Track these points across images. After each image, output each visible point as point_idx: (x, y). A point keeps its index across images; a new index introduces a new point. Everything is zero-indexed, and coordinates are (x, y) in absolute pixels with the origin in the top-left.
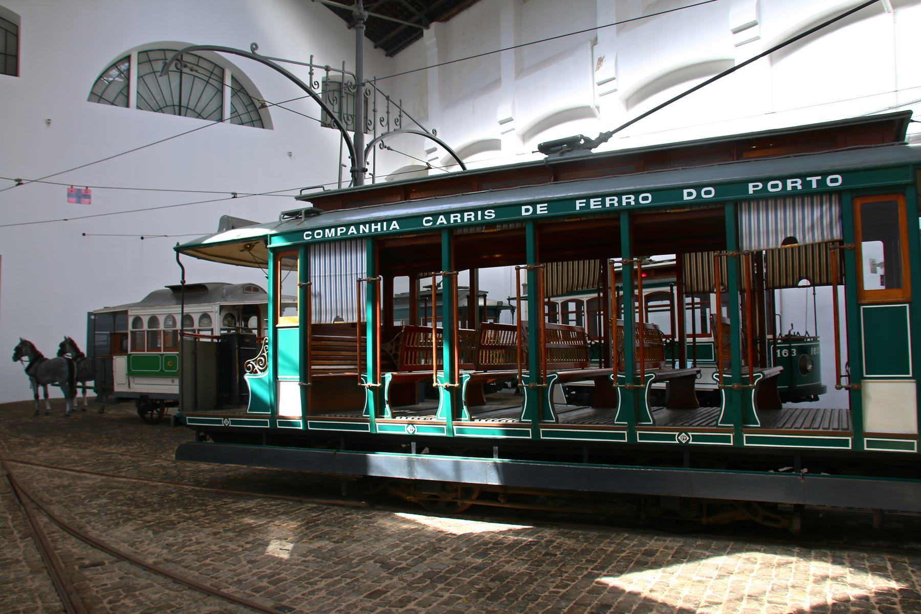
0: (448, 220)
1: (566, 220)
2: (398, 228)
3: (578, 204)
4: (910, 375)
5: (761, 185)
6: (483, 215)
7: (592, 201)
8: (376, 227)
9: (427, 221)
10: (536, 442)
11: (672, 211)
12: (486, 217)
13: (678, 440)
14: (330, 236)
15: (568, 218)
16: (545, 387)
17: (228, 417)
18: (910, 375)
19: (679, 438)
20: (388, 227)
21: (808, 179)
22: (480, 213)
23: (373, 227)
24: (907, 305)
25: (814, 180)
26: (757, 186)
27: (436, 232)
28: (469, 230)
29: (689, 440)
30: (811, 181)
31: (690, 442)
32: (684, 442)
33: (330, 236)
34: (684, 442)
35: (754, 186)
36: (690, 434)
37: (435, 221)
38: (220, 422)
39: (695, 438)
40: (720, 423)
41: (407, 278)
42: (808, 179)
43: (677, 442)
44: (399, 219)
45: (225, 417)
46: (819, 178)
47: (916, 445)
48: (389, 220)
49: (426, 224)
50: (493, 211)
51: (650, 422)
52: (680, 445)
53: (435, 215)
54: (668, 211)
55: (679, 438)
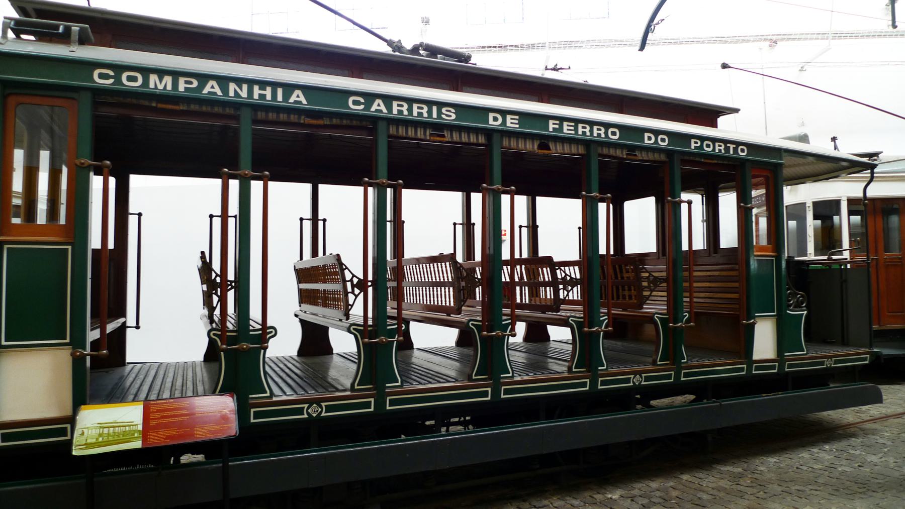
0: (389, 108)
1: (703, 160)
2: (305, 102)
3: (552, 125)
4: (68, 341)
5: (195, 84)
6: (439, 113)
7: (565, 124)
8: (262, 92)
9: (356, 103)
10: (496, 402)
11: (160, 106)
12: (444, 116)
13: (308, 413)
14: (160, 87)
15: (307, 116)
16: (497, 336)
17: (640, 373)
18: (68, 341)
19: (309, 411)
20: (286, 97)
21: (728, 145)
22: (435, 109)
23: (257, 91)
24: (70, 247)
25: (732, 146)
26: (191, 83)
27: (371, 123)
28: (289, 117)
29: (321, 412)
30: (729, 147)
31: (323, 414)
32: (314, 415)
33: (160, 87)
34: (314, 415)
35: (186, 82)
36: (323, 404)
37: (368, 106)
38: (628, 381)
39: (647, 379)
40: (475, 376)
41: (650, 202)
42: (728, 145)
43: (306, 416)
44: (306, 89)
45: (635, 373)
46: (734, 146)
47: (835, 359)
48: (289, 88)
49: (354, 106)
50: (453, 110)
51: (266, 393)
52: (828, 369)
53: (370, 97)
54: (154, 105)
55: (309, 411)
